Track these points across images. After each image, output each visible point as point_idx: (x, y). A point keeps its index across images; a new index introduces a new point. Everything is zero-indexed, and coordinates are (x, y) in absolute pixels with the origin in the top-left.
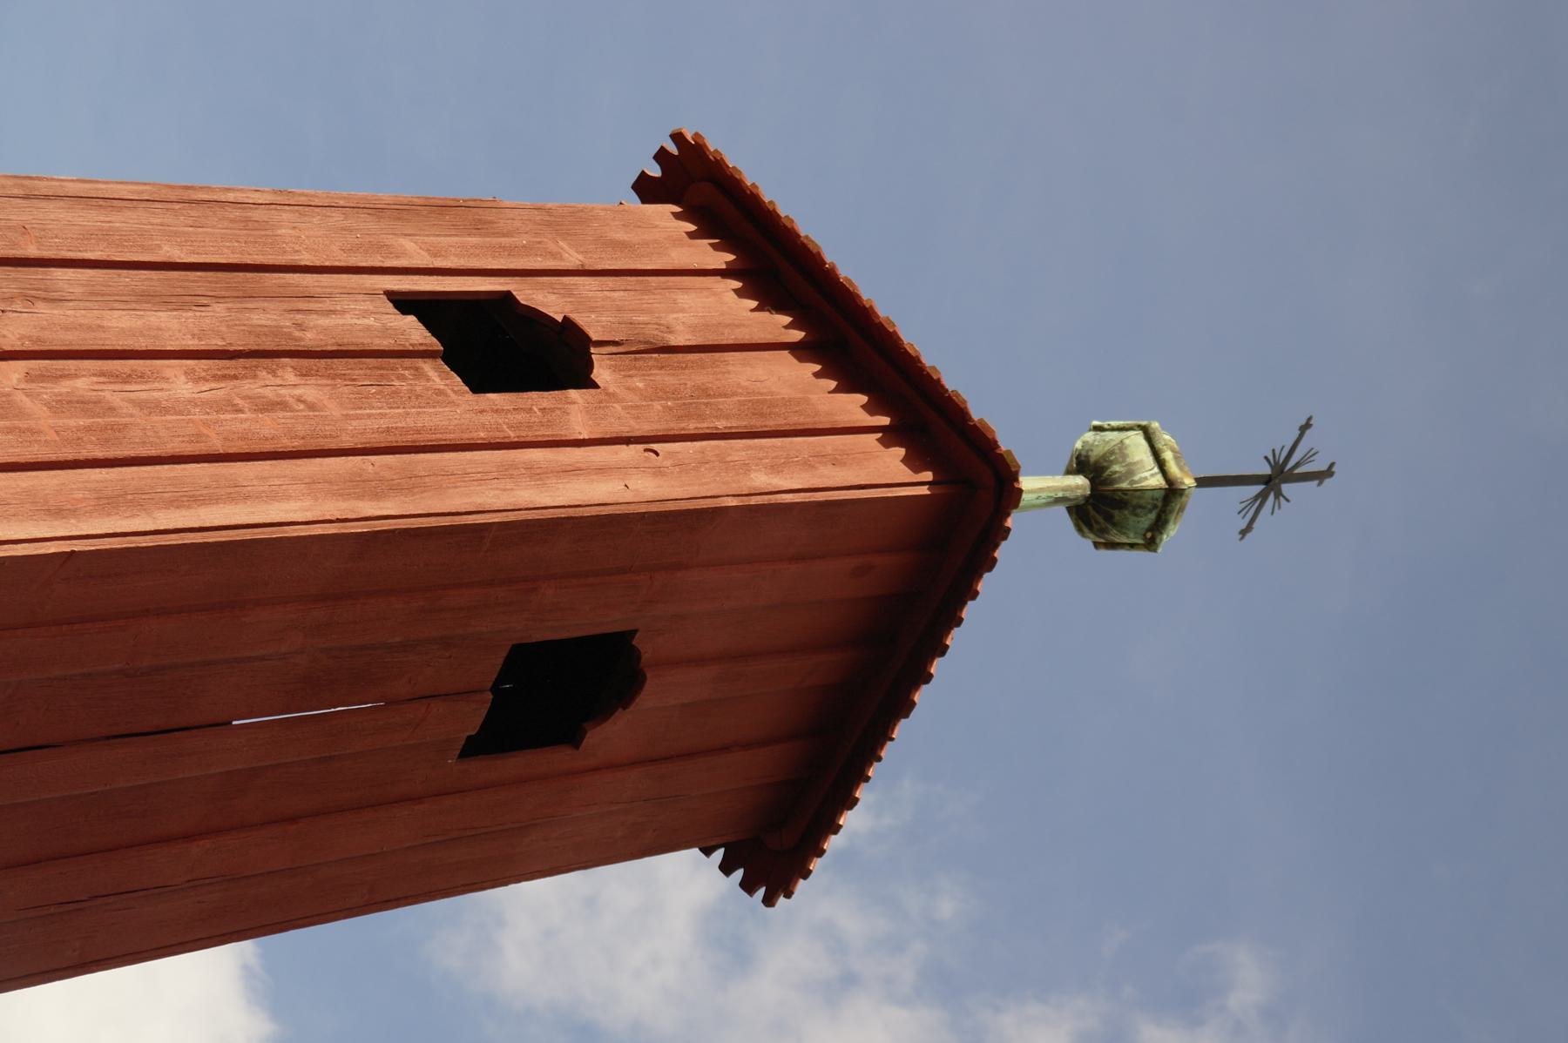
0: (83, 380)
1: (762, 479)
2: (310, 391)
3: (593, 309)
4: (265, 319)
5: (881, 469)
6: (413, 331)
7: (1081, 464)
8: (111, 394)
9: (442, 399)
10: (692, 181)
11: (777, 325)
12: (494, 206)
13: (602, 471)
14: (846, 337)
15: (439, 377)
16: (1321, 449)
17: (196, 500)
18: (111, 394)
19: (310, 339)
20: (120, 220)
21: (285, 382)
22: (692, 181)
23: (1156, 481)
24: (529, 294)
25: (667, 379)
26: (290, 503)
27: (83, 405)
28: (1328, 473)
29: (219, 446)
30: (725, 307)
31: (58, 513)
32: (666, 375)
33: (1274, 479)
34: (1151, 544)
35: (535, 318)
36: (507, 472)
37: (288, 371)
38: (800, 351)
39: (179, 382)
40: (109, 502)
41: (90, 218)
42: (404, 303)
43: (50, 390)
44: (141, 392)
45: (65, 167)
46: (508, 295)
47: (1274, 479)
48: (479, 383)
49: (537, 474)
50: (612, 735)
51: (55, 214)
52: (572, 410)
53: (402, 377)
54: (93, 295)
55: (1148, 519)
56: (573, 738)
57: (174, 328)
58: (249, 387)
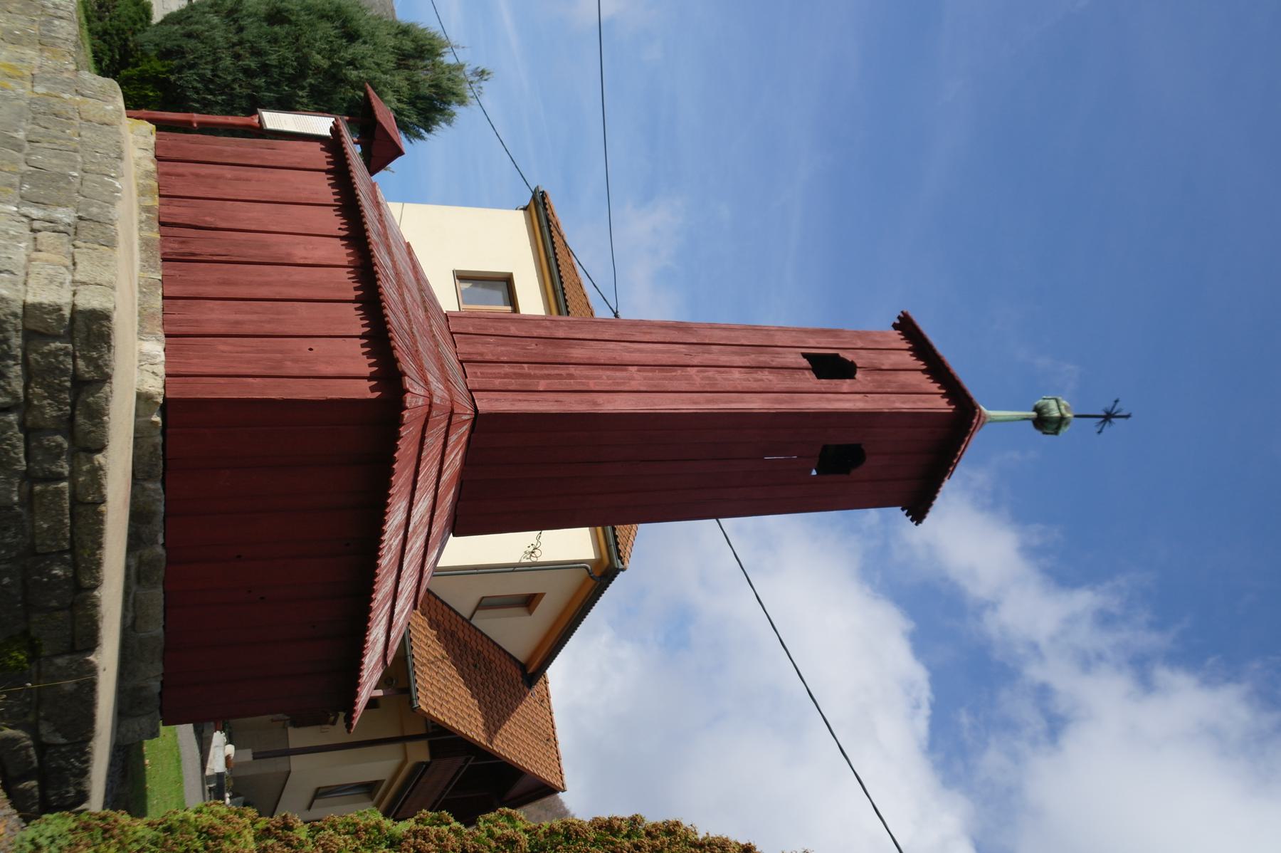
0: (711, 373)
1: (898, 405)
2: (771, 377)
3: (859, 359)
4: (764, 359)
5: (940, 404)
6: (805, 363)
7: (1037, 409)
8: (717, 376)
9: (809, 380)
10: (906, 326)
11: (920, 364)
12: (842, 331)
13: (849, 400)
14: (937, 368)
15: (810, 375)
16: (1123, 408)
17: (732, 402)
18: (717, 376)
19: (774, 364)
20: (733, 334)
21: (765, 375)
22: (906, 326)
23: (1056, 414)
24: (842, 354)
25: (878, 378)
26: (755, 404)
27: (709, 378)
28: (1127, 416)
29: (740, 389)
30: (908, 359)
31: (695, 403)
32: (877, 376)
33: (1108, 417)
34: (1056, 433)
35: (844, 360)
36: (820, 400)
37: (766, 372)
38: (924, 371)
39: (736, 374)
40: (708, 402)
41: (725, 334)
42: (805, 355)
43: (701, 375)
44: (725, 376)
45: (723, 319)
46: (837, 355)
47: (1108, 417)
48: (819, 377)
49: (828, 400)
50: (856, 473)
51: (717, 332)
52: (846, 385)
53: (798, 375)
54: (481, 354)
55: (1055, 426)
56: (848, 472)
57: (738, 360)
58: (755, 376)
